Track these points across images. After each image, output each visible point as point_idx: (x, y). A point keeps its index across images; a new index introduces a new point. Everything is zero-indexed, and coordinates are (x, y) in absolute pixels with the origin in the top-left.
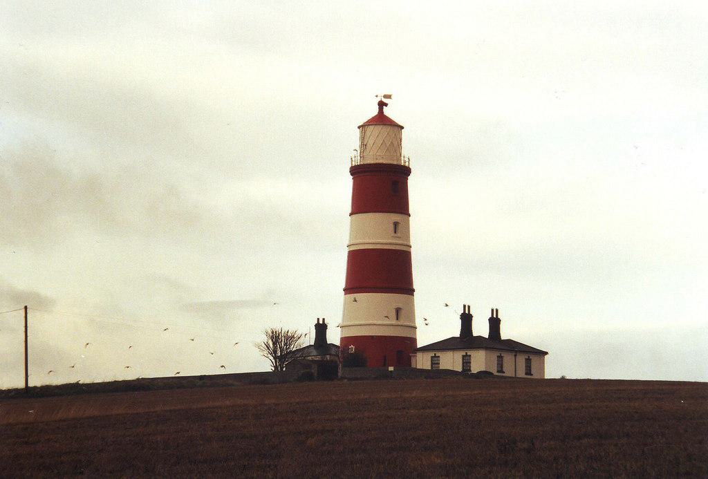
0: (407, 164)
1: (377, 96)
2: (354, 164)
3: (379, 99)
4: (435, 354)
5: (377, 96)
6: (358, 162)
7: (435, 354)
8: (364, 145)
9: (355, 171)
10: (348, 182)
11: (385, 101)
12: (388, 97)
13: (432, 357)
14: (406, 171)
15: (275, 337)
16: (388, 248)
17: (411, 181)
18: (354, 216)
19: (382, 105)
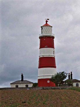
3: (46, 20)
6: (41, 35)
9: (41, 38)
11: (47, 20)
12: (48, 19)
14: (53, 38)
19: (47, 21)
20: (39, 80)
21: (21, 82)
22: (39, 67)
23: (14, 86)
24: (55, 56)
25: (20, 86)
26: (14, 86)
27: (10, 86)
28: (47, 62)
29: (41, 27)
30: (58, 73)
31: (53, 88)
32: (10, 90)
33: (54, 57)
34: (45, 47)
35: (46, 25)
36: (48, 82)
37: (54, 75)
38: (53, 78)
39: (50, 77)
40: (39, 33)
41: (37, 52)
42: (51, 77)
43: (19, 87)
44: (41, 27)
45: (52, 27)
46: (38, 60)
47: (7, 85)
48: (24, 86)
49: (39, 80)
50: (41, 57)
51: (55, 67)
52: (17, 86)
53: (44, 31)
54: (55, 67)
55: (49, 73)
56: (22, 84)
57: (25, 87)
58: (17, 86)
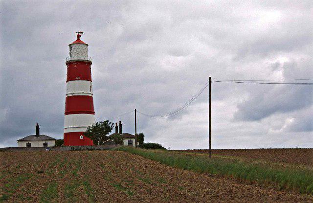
3: (78, 34)
6: (70, 59)
11: (80, 34)
12: (81, 33)
14: (90, 63)
19: (79, 36)
20: (66, 135)
21: (35, 138)
22: (67, 113)
23: (24, 145)
24: (92, 94)
25: (33, 145)
26: (24, 145)
27: (16, 145)
28: (79, 104)
29: (70, 45)
30: (97, 123)
31: (90, 148)
32: (17, 151)
33: (90, 95)
34: (77, 78)
35: (78, 42)
36: (82, 137)
37: (91, 126)
38: (89, 131)
39: (84, 130)
40: (67, 56)
41: (63, 87)
42: (87, 129)
43: (32, 146)
44: (70, 45)
46: (64, 101)
47: (12, 143)
48: (40, 144)
49: (66, 135)
50: (69, 95)
51: (93, 113)
52: (29, 145)
53: (75, 51)
54: (93, 113)
55: (82, 123)
56: (37, 142)
57: (42, 146)
58: (29, 145)
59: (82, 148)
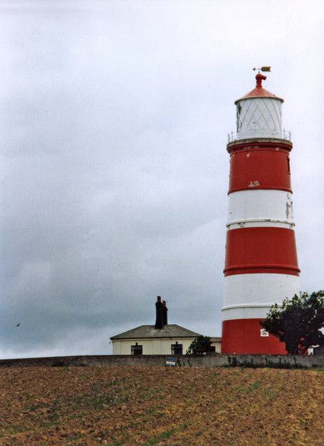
0: (288, 139)
1: (254, 69)
2: (231, 141)
3: (256, 73)
4: (177, 342)
5: (254, 69)
6: (235, 137)
7: (177, 342)
8: (239, 125)
9: (234, 148)
10: (227, 157)
11: (264, 74)
12: (266, 69)
13: (132, 346)
14: (287, 147)
15: (297, 275)
16: (258, 226)
17: (292, 155)
18: (233, 195)
19: (260, 79)
20: (228, 325)
21: (153, 332)
22: (229, 271)
23: (126, 349)
24: (292, 225)
25: (149, 349)
26: (126, 349)
27: (109, 350)
28: (259, 249)
29: (237, 103)
30: (296, 298)
31: (276, 360)
32: (107, 366)
33: (287, 226)
34: (251, 186)
35: (259, 93)
36: (264, 333)
37: (280, 304)
38: (274, 316)
39: (263, 315)
40: (226, 129)
41: (212, 206)
42: (269, 312)
43: (145, 352)
44: (237, 103)
45: (282, 101)
46: (223, 241)
47: (96, 344)
48: (165, 348)
49: (228, 325)
50: (232, 228)
51: (295, 271)
52: (137, 351)
53: (248, 118)
54: (295, 271)
55: (269, 293)
56: (156, 343)
57: (129, 352)
58: (137, 351)
59: (257, 361)
